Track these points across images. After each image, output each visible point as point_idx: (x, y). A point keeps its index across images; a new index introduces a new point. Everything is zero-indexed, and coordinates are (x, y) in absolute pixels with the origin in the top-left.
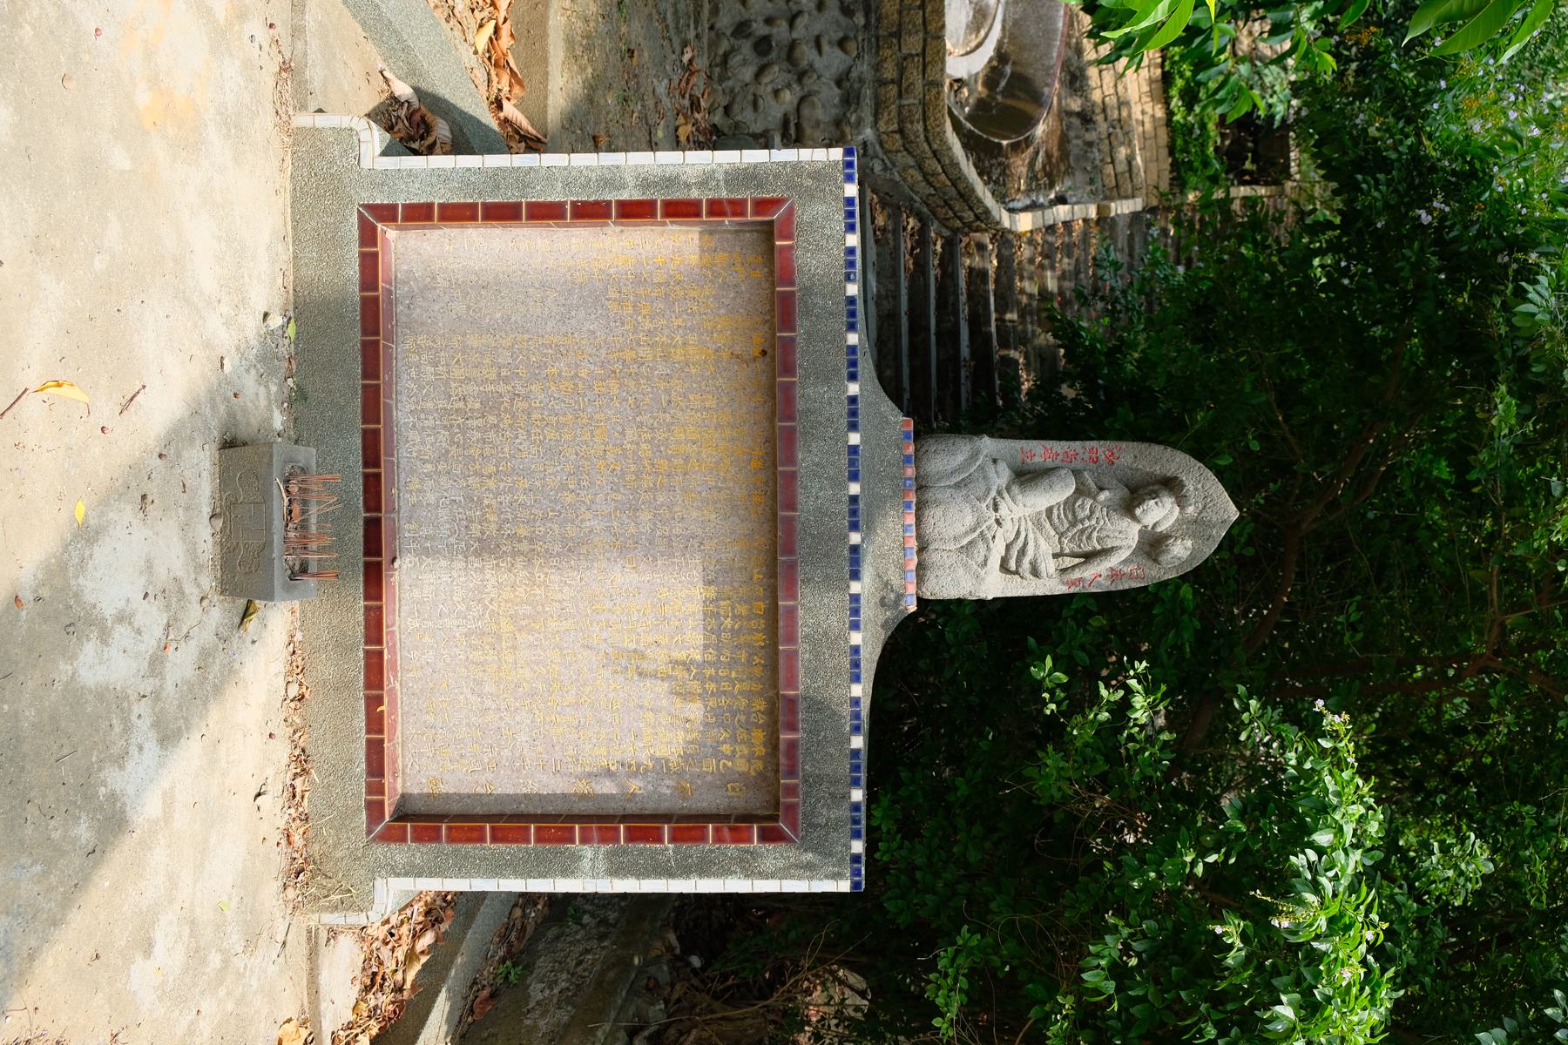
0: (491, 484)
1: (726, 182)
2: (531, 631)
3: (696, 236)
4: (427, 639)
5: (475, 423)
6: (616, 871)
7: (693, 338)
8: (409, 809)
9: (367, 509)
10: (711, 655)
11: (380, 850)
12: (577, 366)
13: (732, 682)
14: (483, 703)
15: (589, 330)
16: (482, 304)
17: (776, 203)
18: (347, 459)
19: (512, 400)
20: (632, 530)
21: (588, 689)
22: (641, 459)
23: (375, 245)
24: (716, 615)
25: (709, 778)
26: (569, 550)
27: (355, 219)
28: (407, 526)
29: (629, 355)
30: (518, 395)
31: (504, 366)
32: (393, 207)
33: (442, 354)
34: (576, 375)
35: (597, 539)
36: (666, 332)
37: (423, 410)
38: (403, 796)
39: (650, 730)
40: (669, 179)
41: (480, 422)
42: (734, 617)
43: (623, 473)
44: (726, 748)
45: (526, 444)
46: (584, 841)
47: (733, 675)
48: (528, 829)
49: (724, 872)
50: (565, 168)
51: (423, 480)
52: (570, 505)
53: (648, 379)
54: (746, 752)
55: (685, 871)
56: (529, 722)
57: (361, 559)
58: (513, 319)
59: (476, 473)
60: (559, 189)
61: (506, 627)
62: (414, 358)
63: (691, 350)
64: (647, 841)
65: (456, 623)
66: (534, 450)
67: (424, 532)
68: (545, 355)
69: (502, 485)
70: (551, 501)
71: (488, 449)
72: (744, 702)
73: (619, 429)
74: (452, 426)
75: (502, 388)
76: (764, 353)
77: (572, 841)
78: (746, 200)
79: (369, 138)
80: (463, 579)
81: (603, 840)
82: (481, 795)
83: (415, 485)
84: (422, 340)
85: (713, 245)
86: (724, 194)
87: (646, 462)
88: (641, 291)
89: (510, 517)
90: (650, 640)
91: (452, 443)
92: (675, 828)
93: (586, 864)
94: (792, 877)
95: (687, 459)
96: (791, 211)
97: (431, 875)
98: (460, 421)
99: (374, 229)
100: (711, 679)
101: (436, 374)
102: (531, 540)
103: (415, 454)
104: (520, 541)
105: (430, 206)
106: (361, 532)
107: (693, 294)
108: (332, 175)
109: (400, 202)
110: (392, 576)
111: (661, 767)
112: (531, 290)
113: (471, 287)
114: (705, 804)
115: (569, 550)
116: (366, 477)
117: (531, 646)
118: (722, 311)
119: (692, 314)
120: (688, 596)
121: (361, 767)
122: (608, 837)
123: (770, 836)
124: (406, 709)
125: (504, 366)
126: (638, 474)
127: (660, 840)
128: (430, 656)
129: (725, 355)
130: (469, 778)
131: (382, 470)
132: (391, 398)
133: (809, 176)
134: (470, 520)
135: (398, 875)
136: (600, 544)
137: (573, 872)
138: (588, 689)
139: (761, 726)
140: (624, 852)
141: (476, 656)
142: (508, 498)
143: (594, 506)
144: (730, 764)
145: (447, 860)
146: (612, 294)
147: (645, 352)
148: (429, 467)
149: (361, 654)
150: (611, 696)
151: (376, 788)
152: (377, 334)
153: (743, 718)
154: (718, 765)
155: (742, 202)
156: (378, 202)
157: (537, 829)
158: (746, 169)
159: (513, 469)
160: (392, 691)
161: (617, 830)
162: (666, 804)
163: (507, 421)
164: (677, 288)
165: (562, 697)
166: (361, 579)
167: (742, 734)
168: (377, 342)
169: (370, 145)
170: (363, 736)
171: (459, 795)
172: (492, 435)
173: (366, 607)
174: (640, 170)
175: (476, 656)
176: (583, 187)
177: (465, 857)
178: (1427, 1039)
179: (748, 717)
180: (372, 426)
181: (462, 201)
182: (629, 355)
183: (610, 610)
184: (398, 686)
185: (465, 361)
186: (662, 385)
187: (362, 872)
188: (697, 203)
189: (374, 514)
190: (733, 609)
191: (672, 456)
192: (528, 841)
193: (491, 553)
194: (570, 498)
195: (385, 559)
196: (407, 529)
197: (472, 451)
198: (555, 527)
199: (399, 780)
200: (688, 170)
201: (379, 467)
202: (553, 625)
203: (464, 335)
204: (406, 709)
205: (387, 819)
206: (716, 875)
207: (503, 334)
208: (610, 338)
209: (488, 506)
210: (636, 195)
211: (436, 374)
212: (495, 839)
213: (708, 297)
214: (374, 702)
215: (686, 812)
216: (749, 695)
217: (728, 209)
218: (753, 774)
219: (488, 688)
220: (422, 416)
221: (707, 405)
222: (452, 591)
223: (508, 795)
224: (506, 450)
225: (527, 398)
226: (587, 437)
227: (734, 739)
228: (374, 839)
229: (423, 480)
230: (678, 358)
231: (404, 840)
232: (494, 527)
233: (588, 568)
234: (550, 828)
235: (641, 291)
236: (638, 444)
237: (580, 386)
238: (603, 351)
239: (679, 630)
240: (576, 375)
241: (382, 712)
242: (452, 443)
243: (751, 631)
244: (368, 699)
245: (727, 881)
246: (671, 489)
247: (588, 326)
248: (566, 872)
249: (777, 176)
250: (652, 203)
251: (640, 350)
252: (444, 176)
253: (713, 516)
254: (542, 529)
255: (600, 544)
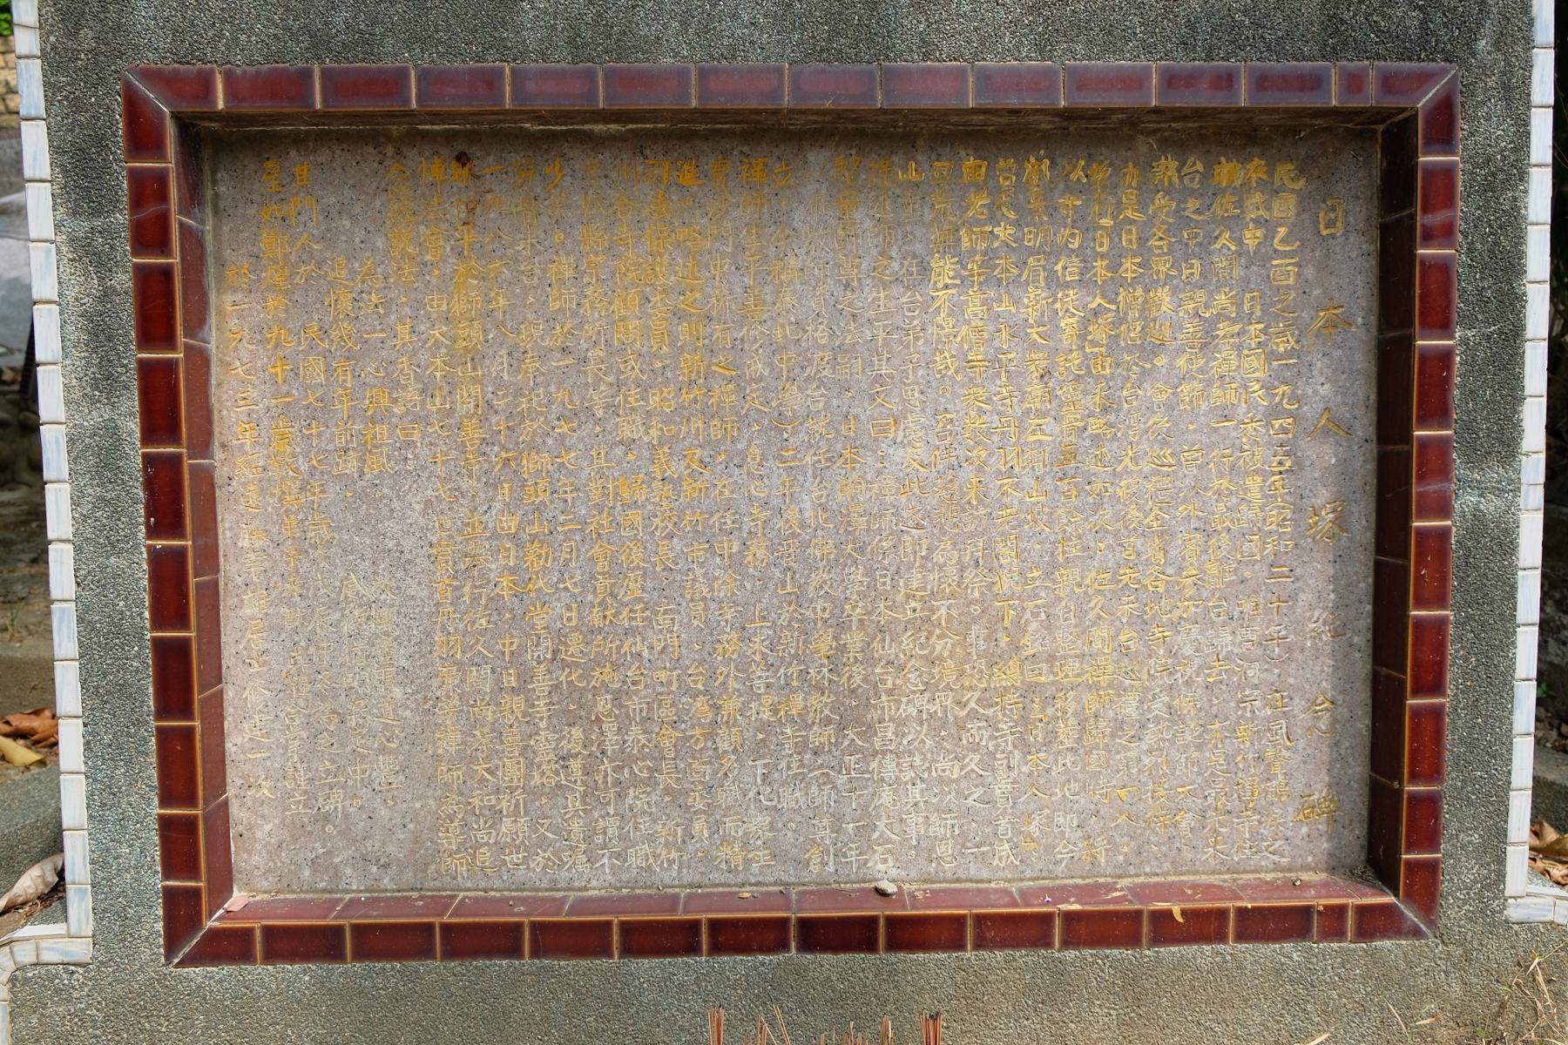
0: (730, 705)
1: (95, 213)
2: (1020, 627)
3: (229, 298)
4: (1033, 829)
5: (611, 737)
6: (1507, 444)
7: (437, 304)
8: (1355, 852)
9: (782, 946)
10: (1068, 268)
11: (1454, 908)
12: (495, 536)
13: (1120, 225)
14: (1157, 720)
15: (424, 512)
16: (376, 723)
17: (134, 107)
18: (681, 986)
19: (565, 665)
20: (819, 426)
21: (1133, 512)
22: (680, 407)
23: (249, 932)
24: (989, 257)
25: (1309, 272)
26: (861, 550)
27: (196, 972)
28: (815, 868)
29: (473, 433)
30: (555, 652)
31: (499, 681)
32: (170, 896)
33: (476, 801)
34: (514, 537)
35: (840, 497)
36: (423, 357)
37: (588, 838)
38: (1332, 870)
39: (1216, 391)
40: (94, 335)
41: (610, 727)
42: (993, 220)
43: (707, 443)
44: (1252, 237)
45: (652, 637)
46: (1444, 509)
47: (1107, 222)
48: (1419, 623)
49: (1513, 223)
50: (78, 550)
51: (724, 839)
52: (771, 549)
53: (519, 392)
54: (1258, 198)
55: (1512, 304)
56: (1195, 629)
57: (882, 957)
58: (403, 663)
59: (711, 735)
60: (123, 563)
61: (1009, 675)
62: (485, 855)
63: (459, 307)
64: (1447, 381)
65: (1002, 773)
66: (663, 621)
67: (825, 834)
68: (475, 599)
69: (732, 684)
70: (765, 588)
71: (663, 712)
72: (1160, 200)
73: (619, 451)
74: (618, 783)
75: (541, 685)
76: (462, 159)
77: (1444, 534)
78: (132, 172)
79: (30, 946)
80: (917, 760)
81: (1444, 471)
82: (1334, 721)
83: (734, 853)
84: (450, 840)
85: (245, 263)
86: (122, 218)
87: (686, 398)
88: (343, 409)
89: (795, 669)
90: (1036, 389)
91: (651, 781)
92: (1424, 325)
93: (1491, 505)
94: (1526, 82)
95: (679, 315)
96: (153, 76)
97: (1503, 813)
98: (607, 765)
99: (214, 934)
100: (1114, 267)
101: (516, 813)
102: (842, 626)
103: (674, 855)
104: (843, 649)
105: (166, 824)
106: (828, 958)
107: (346, 303)
108: (107, 1018)
109: (159, 883)
110: (912, 896)
111: (1290, 370)
112: (347, 628)
113: (343, 745)
114: (1360, 281)
115: (861, 550)
116: (717, 949)
117: (1049, 625)
118: (380, 243)
119: (387, 304)
120: (951, 314)
121: (1290, 952)
122: (1437, 460)
123: (1443, 126)
124: (1167, 866)
125: (499, 681)
126: (709, 414)
127: (1446, 356)
128: (1066, 821)
129: (468, 237)
130: (1302, 743)
131: (704, 917)
132: (563, 900)
133: (73, 33)
134: (802, 747)
135: (1501, 876)
136: (850, 490)
137: (1507, 532)
138: (1133, 512)
139: (1209, 167)
140: (1468, 427)
141: (1067, 732)
142: (760, 677)
143: (775, 502)
144: (1282, 231)
145: (1474, 781)
146: (351, 466)
147: (465, 402)
148: (699, 826)
149: (1071, 954)
150: (1147, 467)
151: (1333, 922)
152: (429, 927)
153: (1192, 204)
154: (1285, 255)
155: (136, 178)
156: (160, 926)
157: (1420, 604)
158: (65, 171)
159: (702, 662)
160: (1138, 892)
161: (1424, 443)
162: (1359, 357)
163: (608, 675)
164: (334, 335)
165: (1148, 563)
166: (920, 956)
167: (1224, 206)
168: (446, 928)
169: (44, 944)
170: (1230, 948)
171: (1332, 763)
172: (634, 704)
173: (978, 946)
174: (77, 395)
175: (1067, 732)
176: (116, 514)
177: (1471, 745)
178: (939, 618)
179: (1191, 193)
180: (616, 937)
181: (153, 759)
182: (473, 433)
183: (980, 470)
184: (1123, 883)
185: (488, 759)
186: (531, 365)
187: (1493, 945)
188: (142, 274)
189: (792, 933)
190: (978, 223)
191: (672, 345)
192: (1441, 623)
193: (868, 705)
194: (758, 551)
195: (881, 911)
196: (820, 868)
197: (667, 743)
198: (815, 579)
199: (1305, 876)
200: (71, 294)
201: (697, 923)
202: (1007, 583)
203: (437, 758)
204: (1167, 866)
205: (1389, 899)
206: (1519, 240)
207: (435, 682)
208: (439, 470)
209: (775, 711)
210: (132, 402)
211: (516, 813)
212: (1437, 688)
213: (353, 272)
214: (1164, 929)
215: (1373, 319)
216: (1146, 192)
217: (152, 209)
218: (1302, 182)
219: (1130, 707)
220: (599, 839)
221: (569, 273)
222: (941, 780)
223: (1336, 668)
224: (663, 676)
225: (560, 636)
226: (636, 516)
227: (1234, 223)
228: (1431, 923)
229: (724, 839)
230: (476, 333)
231: (1432, 868)
232: (815, 701)
233: (897, 514)
234: (1418, 577)
235: (343, 409)
236: (649, 414)
237: (536, 529)
238: (466, 484)
239: (1018, 331)
240: (514, 537)
241: (1184, 913)
242: (651, 781)
243: (1021, 187)
244: (1156, 941)
245: (1532, 217)
246: (739, 347)
247: (415, 514)
248: (1507, 545)
249: (77, 105)
250: (146, 369)
251: (462, 409)
252: (102, 799)
253: (792, 261)
254: (819, 605)
255: (850, 490)
